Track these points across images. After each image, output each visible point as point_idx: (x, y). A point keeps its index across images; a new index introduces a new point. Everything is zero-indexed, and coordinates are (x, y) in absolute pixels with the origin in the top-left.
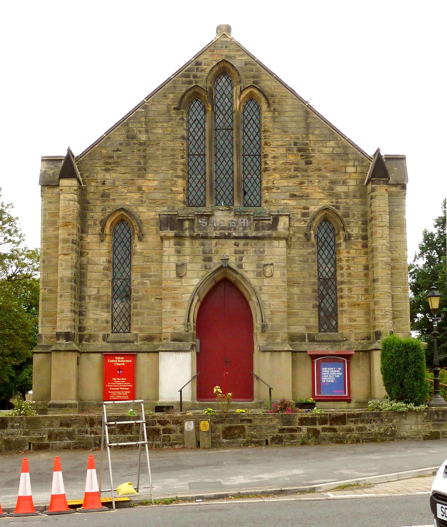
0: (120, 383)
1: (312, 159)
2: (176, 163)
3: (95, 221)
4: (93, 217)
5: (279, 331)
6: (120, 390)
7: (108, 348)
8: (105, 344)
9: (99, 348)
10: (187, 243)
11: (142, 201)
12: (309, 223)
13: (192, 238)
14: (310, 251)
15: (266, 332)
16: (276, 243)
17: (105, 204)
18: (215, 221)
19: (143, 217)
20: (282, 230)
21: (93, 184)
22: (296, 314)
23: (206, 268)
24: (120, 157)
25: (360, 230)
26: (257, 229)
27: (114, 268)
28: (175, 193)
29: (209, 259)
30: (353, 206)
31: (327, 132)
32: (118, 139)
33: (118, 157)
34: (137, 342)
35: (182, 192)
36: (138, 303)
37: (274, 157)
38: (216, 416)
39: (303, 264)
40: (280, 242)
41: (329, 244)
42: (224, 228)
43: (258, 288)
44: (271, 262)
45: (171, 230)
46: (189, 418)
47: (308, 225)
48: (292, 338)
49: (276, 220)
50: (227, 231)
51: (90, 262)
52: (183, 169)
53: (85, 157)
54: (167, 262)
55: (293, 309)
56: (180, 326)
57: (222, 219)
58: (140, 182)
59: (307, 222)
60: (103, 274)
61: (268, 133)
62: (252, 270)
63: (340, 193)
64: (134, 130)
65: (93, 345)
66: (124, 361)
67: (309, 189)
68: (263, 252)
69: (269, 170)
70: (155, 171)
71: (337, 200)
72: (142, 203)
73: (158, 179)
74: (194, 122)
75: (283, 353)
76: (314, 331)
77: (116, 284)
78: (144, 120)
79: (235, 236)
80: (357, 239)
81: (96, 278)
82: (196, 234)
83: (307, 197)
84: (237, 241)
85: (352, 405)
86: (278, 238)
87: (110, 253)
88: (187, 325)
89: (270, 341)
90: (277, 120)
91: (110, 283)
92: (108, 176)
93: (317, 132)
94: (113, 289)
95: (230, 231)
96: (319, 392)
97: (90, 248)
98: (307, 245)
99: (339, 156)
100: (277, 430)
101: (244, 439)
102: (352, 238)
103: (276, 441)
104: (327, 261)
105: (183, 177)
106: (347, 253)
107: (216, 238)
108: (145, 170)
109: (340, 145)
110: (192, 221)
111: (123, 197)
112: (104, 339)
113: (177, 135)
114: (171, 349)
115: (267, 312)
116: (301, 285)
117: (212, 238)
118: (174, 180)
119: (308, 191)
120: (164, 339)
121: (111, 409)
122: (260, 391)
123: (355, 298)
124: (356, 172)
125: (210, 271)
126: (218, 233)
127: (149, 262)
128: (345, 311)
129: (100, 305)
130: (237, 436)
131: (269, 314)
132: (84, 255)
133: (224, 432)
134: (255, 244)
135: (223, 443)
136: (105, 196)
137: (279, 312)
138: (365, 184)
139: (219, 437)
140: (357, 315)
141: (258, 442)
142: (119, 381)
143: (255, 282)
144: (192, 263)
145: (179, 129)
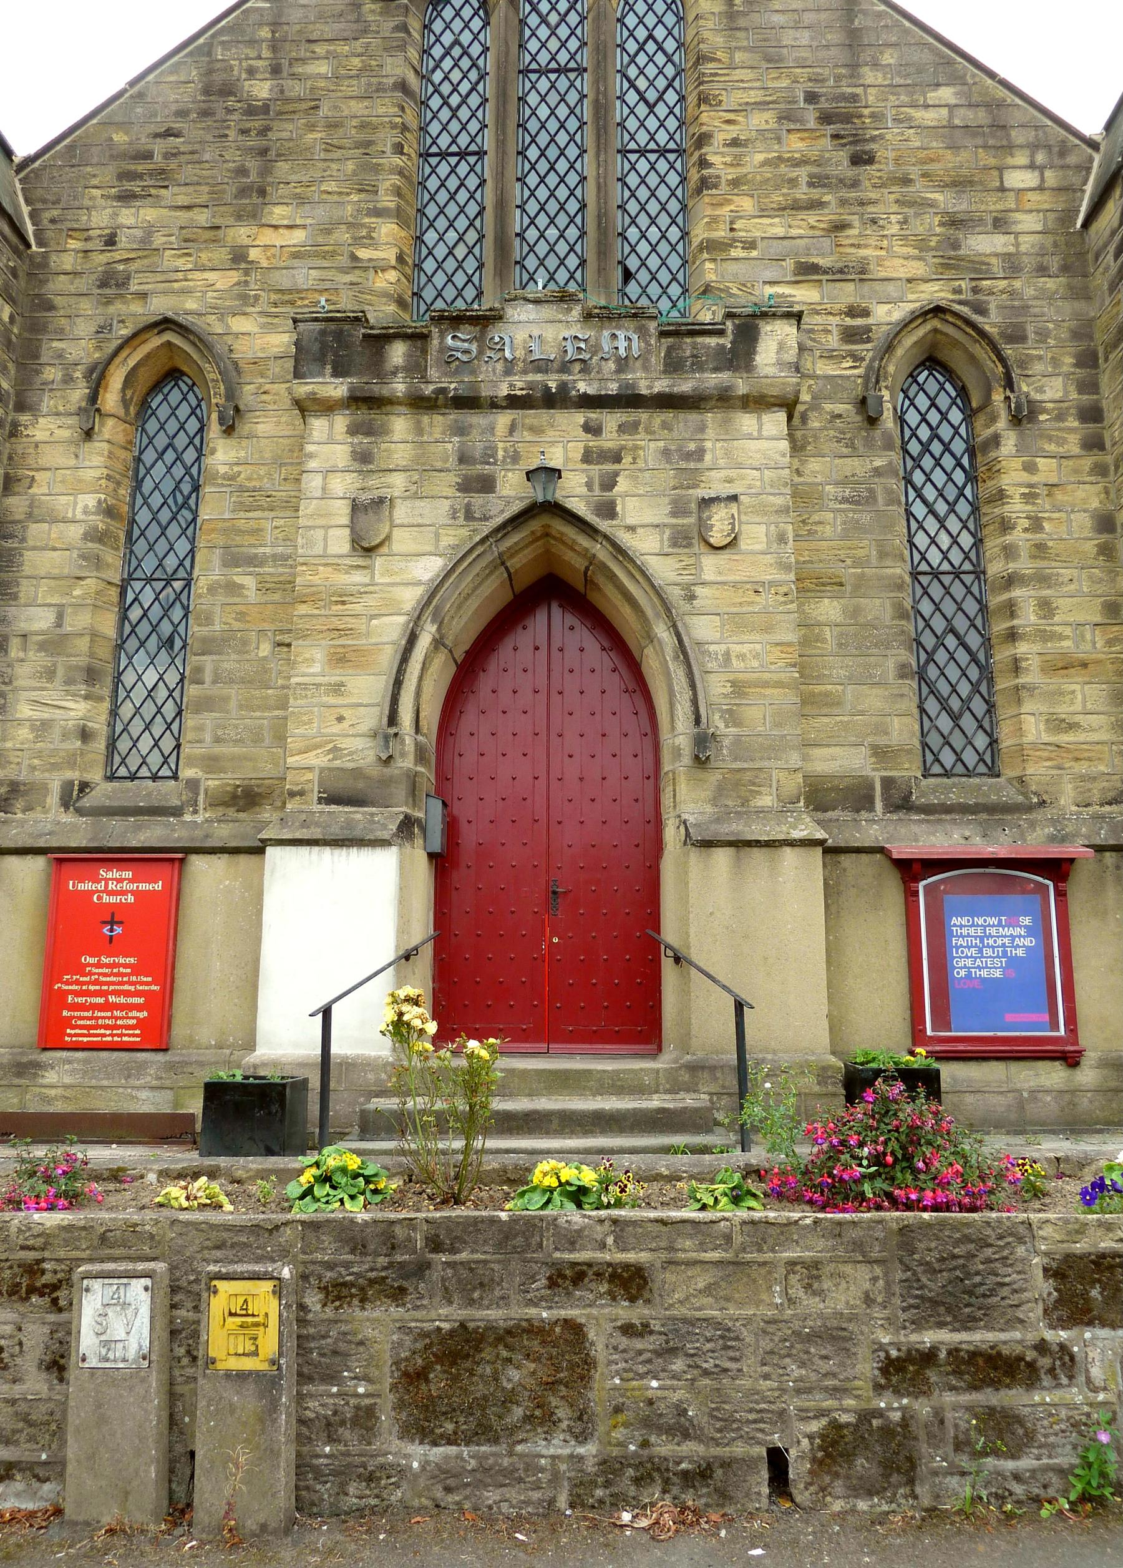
0: (111, 978)
1: (873, 146)
2: (376, 169)
3: (68, 368)
4: (60, 356)
5: (766, 764)
6: (107, 1007)
7: (78, 832)
8: (68, 818)
9: (40, 836)
10: (400, 425)
11: (244, 298)
12: (872, 360)
13: (420, 403)
14: (878, 463)
15: (713, 764)
16: (747, 422)
17: (111, 309)
18: (507, 340)
19: (244, 350)
20: (771, 371)
21: (73, 244)
22: (830, 702)
23: (469, 516)
24: (174, 155)
25: (1072, 388)
26: (673, 366)
27: (130, 541)
28: (366, 269)
29: (486, 485)
30: (1039, 303)
31: (926, 57)
32: (172, 97)
33: (168, 156)
34: (195, 812)
35: (393, 262)
36: (208, 662)
37: (735, 143)
38: (352, 1237)
39: (854, 511)
40: (767, 418)
41: (947, 448)
42: (541, 366)
43: (675, 594)
44: (732, 492)
45: (336, 374)
46: (116, 1249)
47: (869, 368)
48: (820, 796)
49: (747, 328)
50: (555, 376)
51: (36, 511)
52: (399, 187)
53: (53, 157)
54: (319, 494)
55: (820, 679)
56: (359, 743)
57: (535, 333)
58: (241, 234)
59: (863, 359)
60: (80, 556)
61: (710, 65)
62: (656, 522)
63: (987, 260)
64: (231, 68)
65: (22, 823)
66: (134, 887)
67: (866, 246)
68: (700, 454)
69: (716, 186)
70: (297, 196)
71: (974, 284)
72: (246, 304)
73: (309, 221)
74: (447, 53)
75: (788, 850)
76: (908, 769)
77: (135, 599)
78: (270, 35)
79: (585, 394)
80: (1060, 417)
81: (56, 571)
82: (431, 387)
83: (862, 272)
84: (593, 415)
85: (1087, 1075)
86: (757, 403)
87: (118, 484)
88: (386, 738)
89: (730, 803)
90: (742, 22)
91: (114, 593)
92: (126, 216)
93: (889, 58)
94: (124, 617)
95: (565, 377)
96: (942, 1018)
97: (42, 462)
98: (869, 443)
99: (974, 135)
100: (866, 1368)
101: (582, 1437)
102: (1042, 417)
103: (860, 1462)
104: (941, 508)
105: (399, 215)
106: (1024, 469)
107: (514, 402)
108: (262, 192)
109: (976, 98)
110: (419, 338)
111: (176, 285)
112: (66, 802)
113: (384, 80)
114: (316, 833)
115: (716, 687)
116: (849, 588)
117: (494, 405)
118: (363, 225)
119: (863, 252)
120: (292, 794)
121: (66, 1087)
122: (695, 1013)
123: (1067, 637)
124: (1040, 188)
125: (486, 528)
126: (519, 385)
127: (261, 508)
128: (1031, 689)
129: (60, 672)
130: (518, 1412)
131: (726, 696)
132: (16, 489)
133: (412, 1378)
134: (665, 426)
135: (402, 1471)
136: (112, 282)
137: (766, 684)
138: (1078, 225)
139: (364, 1419)
140: (1078, 707)
141: (701, 1474)
142: (107, 966)
143: (665, 570)
144: (416, 496)
145: (389, 60)
